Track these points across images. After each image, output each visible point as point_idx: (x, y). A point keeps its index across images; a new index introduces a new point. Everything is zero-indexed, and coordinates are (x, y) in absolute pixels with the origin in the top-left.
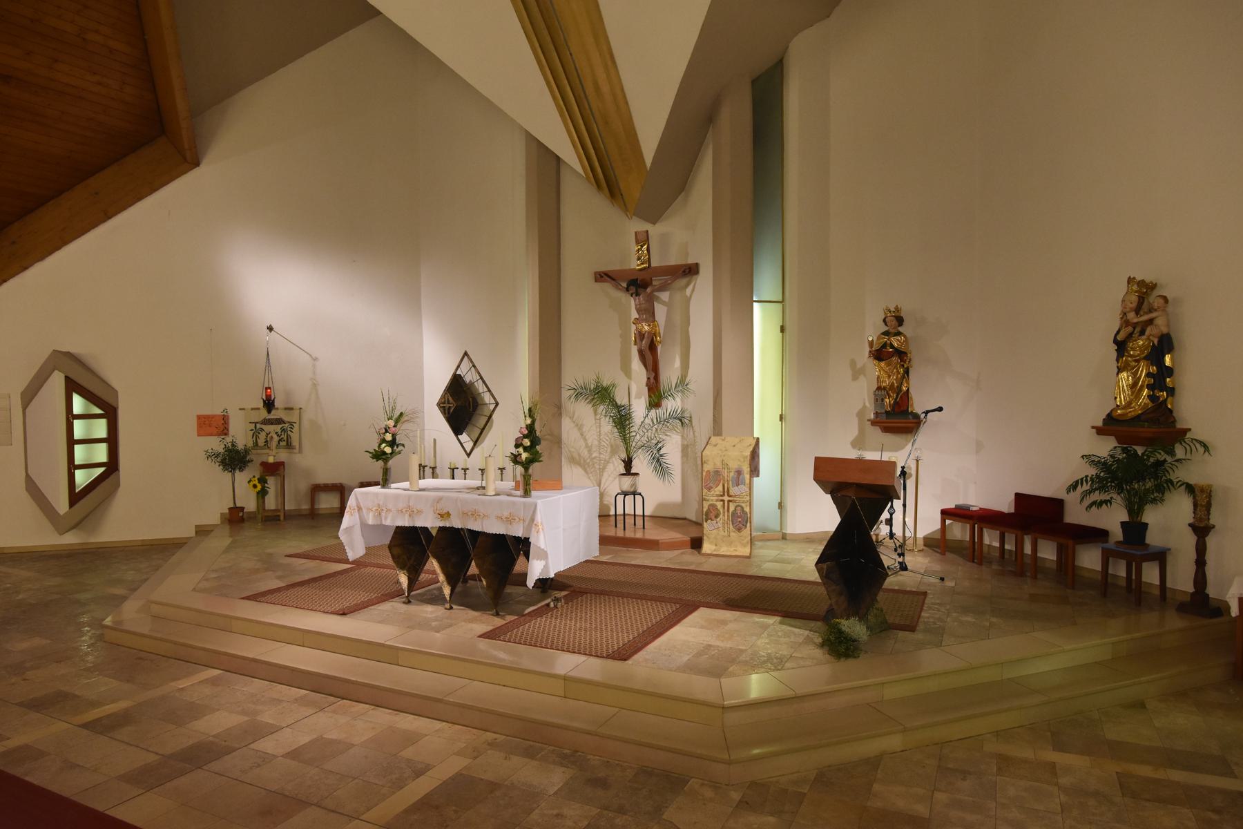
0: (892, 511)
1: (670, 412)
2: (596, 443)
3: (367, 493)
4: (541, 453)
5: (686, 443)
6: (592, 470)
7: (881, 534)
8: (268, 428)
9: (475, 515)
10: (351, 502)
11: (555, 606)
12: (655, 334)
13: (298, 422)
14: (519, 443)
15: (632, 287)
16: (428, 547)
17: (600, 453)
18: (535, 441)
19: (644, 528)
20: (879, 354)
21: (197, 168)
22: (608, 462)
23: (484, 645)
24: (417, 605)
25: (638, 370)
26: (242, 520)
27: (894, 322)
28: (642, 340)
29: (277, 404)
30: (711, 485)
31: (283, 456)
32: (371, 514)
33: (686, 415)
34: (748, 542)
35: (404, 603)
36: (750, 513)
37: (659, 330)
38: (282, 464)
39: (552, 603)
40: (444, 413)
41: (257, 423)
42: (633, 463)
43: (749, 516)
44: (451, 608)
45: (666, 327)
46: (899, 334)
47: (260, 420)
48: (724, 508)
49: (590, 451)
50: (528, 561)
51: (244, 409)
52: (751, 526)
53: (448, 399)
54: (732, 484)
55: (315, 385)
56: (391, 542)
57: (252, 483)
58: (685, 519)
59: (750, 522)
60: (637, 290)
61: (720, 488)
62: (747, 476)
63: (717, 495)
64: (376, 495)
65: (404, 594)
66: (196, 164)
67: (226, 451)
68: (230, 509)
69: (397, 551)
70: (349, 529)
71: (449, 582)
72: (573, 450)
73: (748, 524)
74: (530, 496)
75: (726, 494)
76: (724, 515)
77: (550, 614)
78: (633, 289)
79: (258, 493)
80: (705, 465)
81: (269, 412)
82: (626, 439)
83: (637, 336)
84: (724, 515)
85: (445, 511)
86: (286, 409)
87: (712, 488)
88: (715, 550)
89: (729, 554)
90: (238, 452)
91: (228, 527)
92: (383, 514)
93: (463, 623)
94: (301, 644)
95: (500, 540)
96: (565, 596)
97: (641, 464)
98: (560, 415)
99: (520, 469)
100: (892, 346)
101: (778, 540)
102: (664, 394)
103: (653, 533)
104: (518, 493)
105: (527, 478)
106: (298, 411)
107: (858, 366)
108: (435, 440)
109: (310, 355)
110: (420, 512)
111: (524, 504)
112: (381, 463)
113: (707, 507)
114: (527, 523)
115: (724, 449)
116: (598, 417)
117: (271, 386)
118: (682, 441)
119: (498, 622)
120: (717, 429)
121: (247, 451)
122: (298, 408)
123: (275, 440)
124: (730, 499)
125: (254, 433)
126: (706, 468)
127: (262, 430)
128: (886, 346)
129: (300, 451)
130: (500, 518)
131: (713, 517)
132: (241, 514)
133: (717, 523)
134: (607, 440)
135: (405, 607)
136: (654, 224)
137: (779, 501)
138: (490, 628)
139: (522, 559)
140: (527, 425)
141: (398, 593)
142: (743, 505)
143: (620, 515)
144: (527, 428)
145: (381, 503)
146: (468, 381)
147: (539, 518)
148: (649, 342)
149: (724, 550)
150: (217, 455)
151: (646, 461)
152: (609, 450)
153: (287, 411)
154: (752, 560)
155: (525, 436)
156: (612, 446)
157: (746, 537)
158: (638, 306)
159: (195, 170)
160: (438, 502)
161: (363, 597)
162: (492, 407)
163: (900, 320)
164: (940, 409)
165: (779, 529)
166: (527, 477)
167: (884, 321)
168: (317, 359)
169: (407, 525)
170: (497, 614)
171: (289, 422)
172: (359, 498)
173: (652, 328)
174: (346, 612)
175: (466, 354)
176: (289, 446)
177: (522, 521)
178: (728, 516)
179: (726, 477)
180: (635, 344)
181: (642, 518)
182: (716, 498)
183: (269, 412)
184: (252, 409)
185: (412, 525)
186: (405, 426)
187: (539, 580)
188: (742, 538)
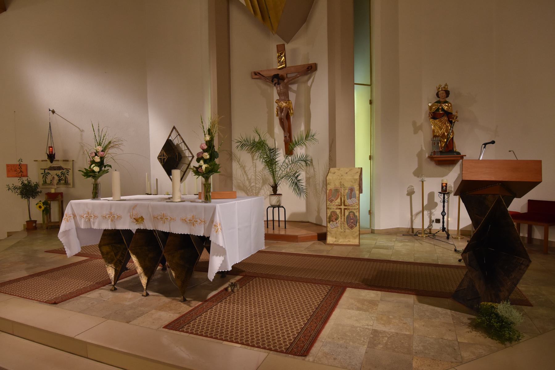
0: (444, 214)
1: (300, 157)
2: (253, 177)
3: (79, 204)
4: (219, 165)
5: (308, 176)
6: (252, 193)
7: (432, 228)
8: (53, 173)
9: (163, 218)
10: (68, 211)
11: (232, 291)
12: (289, 109)
13: (72, 169)
14: (200, 157)
15: (275, 79)
16: (128, 248)
17: (256, 184)
18: (213, 155)
19: (285, 228)
20: (435, 115)
21: (5, 12)
22: (261, 189)
23: (169, 336)
24: (122, 292)
25: (278, 131)
26: (35, 228)
27: (444, 94)
28: (281, 112)
29: (56, 158)
30: (332, 198)
31: (62, 189)
32: (83, 220)
33: (309, 158)
34: (357, 236)
35: (111, 290)
36: (359, 217)
37: (292, 106)
38: (61, 194)
39: (230, 288)
40: (161, 162)
41: (46, 169)
42: (278, 188)
43: (358, 218)
44: (147, 295)
45: (295, 104)
46: (446, 102)
47: (48, 167)
48: (341, 213)
49: (250, 182)
50: (209, 253)
51: (37, 161)
52: (359, 225)
53: (163, 153)
54: (347, 197)
55: (82, 147)
56: (100, 242)
57: (38, 205)
58: (308, 222)
59: (359, 223)
60: (278, 81)
61: (339, 200)
62: (357, 192)
63: (337, 205)
64: (86, 204)
65: (111, 283)
66: (5, 10)
67: (22, 186)
68: (27, 222)
69: (106, 249)
70: (66, 232)
71: (146, 274)
72: (239, 181)
73: (358, 224)
74: (210, 202)
75: (343, 204)
76: (341, 219)
77: (228, 298)
78: (276, 80)
79: (43, 211)
80: (328, 186)
81: (52, 162)
82: (273, 173)
83: (279, 110)
84: (341, 219)
85: (139, 216)
86: (64, 161)
87: (333, 201)
88: (335, 241)
89: (344, 243)
90: (31, 186)
91: (27, 232)
92: (92, 220)
93: (154, 311)
94: (11, 333)
95: (186, 239)
96: (238, 281)
97: (284, 188)
98: (231, 159)
99: (201, 179)
100: (443, 109)
101: (369, 233)
102: (298, 142)
103: (290, 231)
104: (200, 200)
105: (206, 186)
106: (72, 162)
107: (418, 125)
108: (157, 179)
109: (79, 128)
110: (119, 217)
111: (205, 208)
112: (91, 180)
113: (330, 213)
114: (207, 224)
115: (341, 175)
116: (254, 161)
117: (52, 146)
118: (306, 175)
119: (185, 308)
120: (332, 162)
121: (37, 185)
122: (72, 160)
123: (56, 179)
124: (346, 207)
125: (44, 175)
126: (329, 187)
127: (49, 173)
128: (439, 110)
129: (74, 186)
130: (184, 221)
131: (334, 220)
132: (34, 225)
133: (336, 223)
134: (260, 176)
135: (111, 295)
136: (288, 43)
137: (369, 210)
138: (176, 316)
139: (205, 250)
140: (206, 142)
141: (104, 282)
142: (355, 211)
143: (271, 221)
144: (206, 144)
145: (90, 211)
146: (176, 144)
147: (217, 219)
148: (286, 114)
149: (341, 241)
150: (15, 188)
151: (288, 186)
152: (261, 182)
153: (64, 162)
154: (361, 247)
155: (205, 151)
156: (263, 179)
157: (356, 232)
158: (279, 91)
159: (3, 13)
160: (133, 209)
161: (82, 284)
162: (190, 159)
163: (447, 93)
164: (493, 142)
165: (369, 227)
166: (207, 186)
167: (437, 95)
168: (83, 130)
169: (110, 228)
170: (184, 300)
171: (66, 169)
172: (74, 208)
173: (288, 105)
174: (57, 302)
175: (174, 128)
176: (66, 183)
177: (203, 223)
178: (344, 219)
179: (343, 193)
180: (277, 115)
181: (272, 222)
182: (336, 207)
183: (52, 162)
184: (42, 161)
185: (113, 229)
186: (110, 151)
187: (218, 273)
188: (354, 233)
